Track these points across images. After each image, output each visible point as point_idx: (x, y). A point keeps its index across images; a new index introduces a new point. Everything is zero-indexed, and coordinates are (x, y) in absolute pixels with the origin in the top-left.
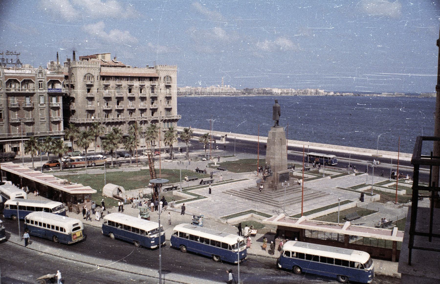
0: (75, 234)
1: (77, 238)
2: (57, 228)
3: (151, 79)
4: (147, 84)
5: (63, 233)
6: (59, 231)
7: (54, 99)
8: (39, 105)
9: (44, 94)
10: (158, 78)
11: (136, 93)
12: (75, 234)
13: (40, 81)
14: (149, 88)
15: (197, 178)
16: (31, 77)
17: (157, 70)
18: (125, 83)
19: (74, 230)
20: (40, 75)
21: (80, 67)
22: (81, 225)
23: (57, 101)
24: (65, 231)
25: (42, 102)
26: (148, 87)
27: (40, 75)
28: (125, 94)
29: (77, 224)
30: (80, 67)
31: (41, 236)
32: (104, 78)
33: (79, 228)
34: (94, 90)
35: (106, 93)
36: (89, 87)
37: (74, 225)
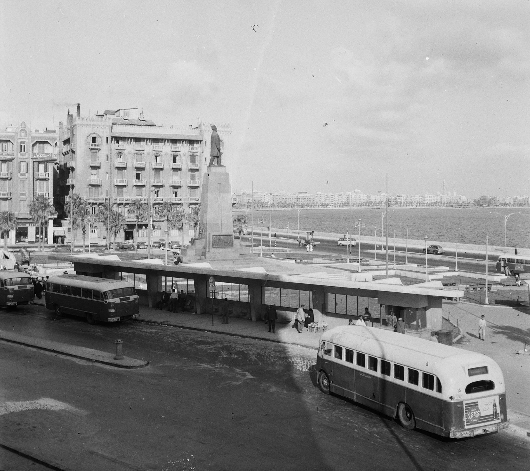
0: (475, 405)
1: (483, 419)
2: (414, 376)
3: (192, 142)
4: (184, 149)
5: (433, 393)
6: (420, 388)
7: (42, 166)
8: (19, 174)
9: (27, 160)
10: (201, 141)
11: (167, 163)
12: (475, 405)
13: (21, 142)
14: (187, 155)
15: (454, 282)
16: (10, 137)
17: (201, 131)
18: (148, 148)
19: (471, 388)
20: (23, 134)
21: (81, 125)
22: (494, 375)
23: (46, 170)
24: (439, 390)
25: (23, 170)
26: (184, 155)
27: (23, 134)
28: (150, 163)
29: (484, 370)
30: (81, 125)
31: (354, 394)
32: (117, 139)
33: (488, 385)
34: (101, 156)
35: (119, 162)
36: (94, 150)
37: (472, 372)
